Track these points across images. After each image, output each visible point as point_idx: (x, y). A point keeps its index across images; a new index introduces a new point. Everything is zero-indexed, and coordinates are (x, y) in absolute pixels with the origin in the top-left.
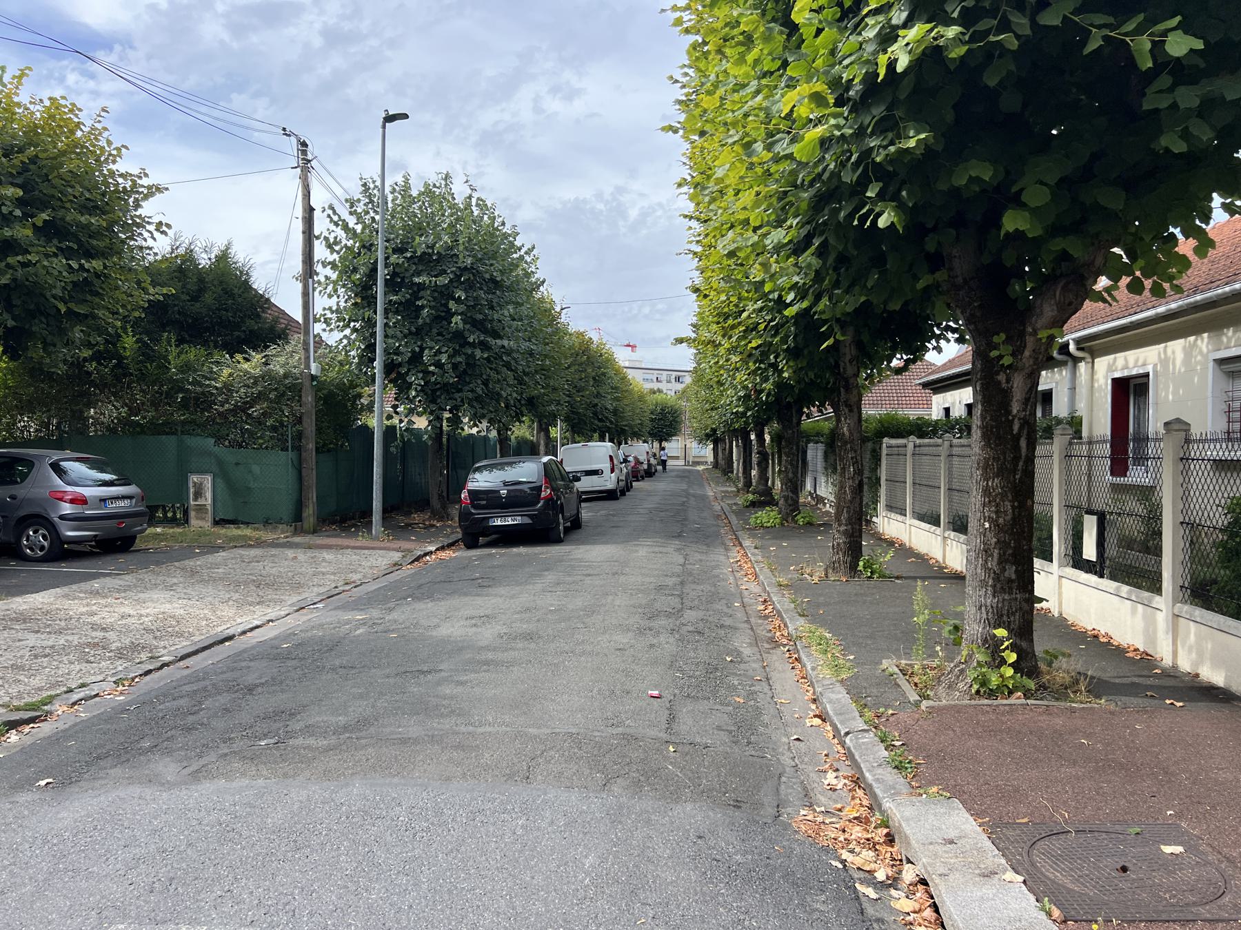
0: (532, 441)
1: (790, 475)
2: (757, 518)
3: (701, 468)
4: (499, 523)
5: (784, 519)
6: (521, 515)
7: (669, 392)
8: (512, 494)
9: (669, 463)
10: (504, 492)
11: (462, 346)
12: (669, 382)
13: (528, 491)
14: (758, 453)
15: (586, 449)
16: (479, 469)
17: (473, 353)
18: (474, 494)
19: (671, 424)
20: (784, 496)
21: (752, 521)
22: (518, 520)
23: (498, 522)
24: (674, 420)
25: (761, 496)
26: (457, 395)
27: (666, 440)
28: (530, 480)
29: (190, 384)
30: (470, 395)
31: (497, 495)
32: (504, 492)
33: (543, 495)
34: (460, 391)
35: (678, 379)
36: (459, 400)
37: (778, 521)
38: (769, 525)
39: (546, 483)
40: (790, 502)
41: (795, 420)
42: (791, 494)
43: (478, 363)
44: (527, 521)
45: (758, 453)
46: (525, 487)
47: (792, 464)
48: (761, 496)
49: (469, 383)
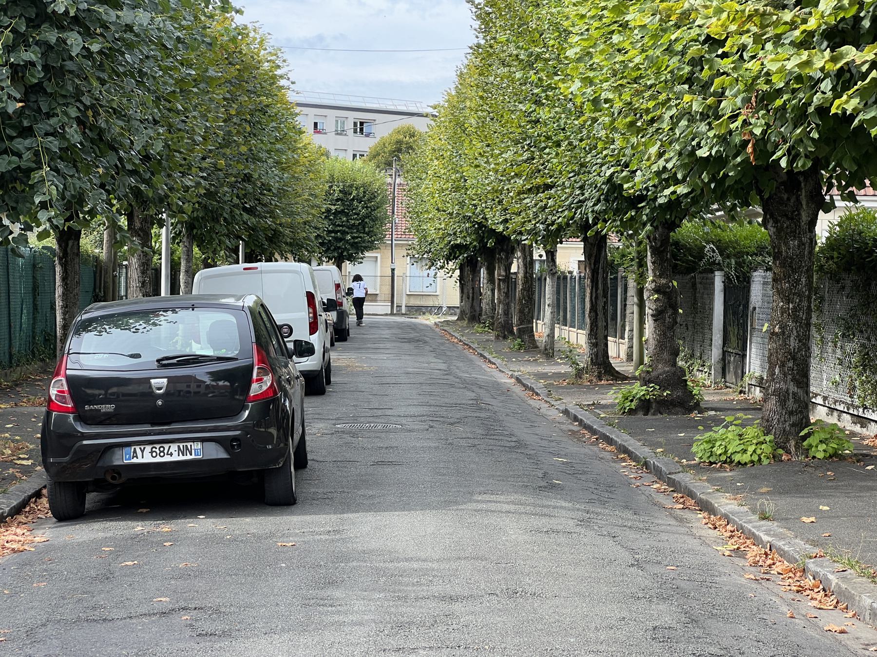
0: (96, 259)
1: (793, 343)
2: (712, 442)
3: (430, 320)
4: (176, 458)
5: (780, 444)
6: (203, 440)
7: (341, 155)
8: (182, 387)
9: (367, 308)
10: (159, 383)
11: (34, 24)
12: (341, 133)
13: (207, 380)
14: (657, 290)
15: (250, 276)
16: (85, 326)
17: (62, 41)
18: (78, 386)
19: (363, 224)
20: (777, 393)
21: (699, 449)
22: (196, 452)
23: (145, 456)
24: (367, 216)
25: (663, 388)
26: (20, 144)
27: (351, 258)
28: (223, 353)
29: (205, 14)
30: (54, 144)
31: (142, 388)
32: (159, 383)
33: (255, 389)
34: (27, 132)
35: (360, 128)
36: (27, 155)
37: (767, 449)
38: (746, 458)
39: (261, 361)
40: (791, 404)
41: (805, 217)
42: (793, 388)
43: (69, 65)
44: (216, 452)
45: (657, 290)
46: (200, 373)
47: (796, 318)
48: (663, 388)
49: (49, 116)
